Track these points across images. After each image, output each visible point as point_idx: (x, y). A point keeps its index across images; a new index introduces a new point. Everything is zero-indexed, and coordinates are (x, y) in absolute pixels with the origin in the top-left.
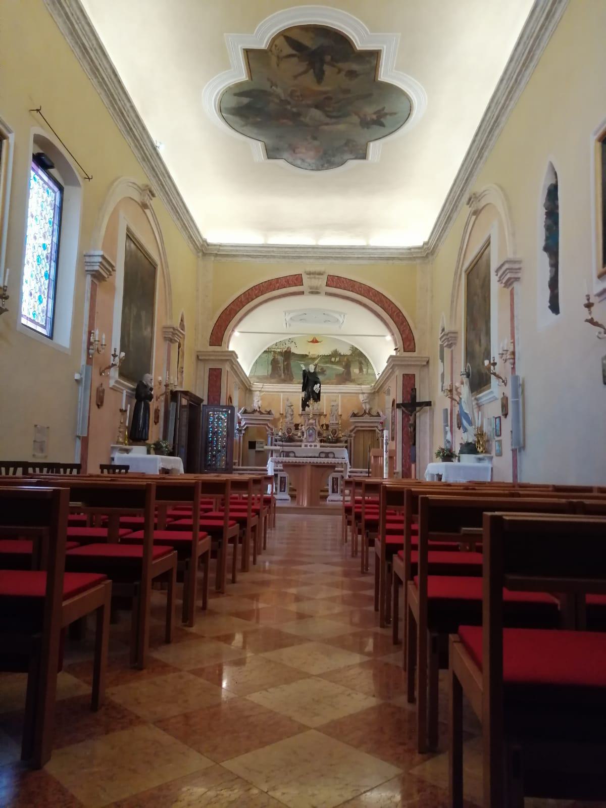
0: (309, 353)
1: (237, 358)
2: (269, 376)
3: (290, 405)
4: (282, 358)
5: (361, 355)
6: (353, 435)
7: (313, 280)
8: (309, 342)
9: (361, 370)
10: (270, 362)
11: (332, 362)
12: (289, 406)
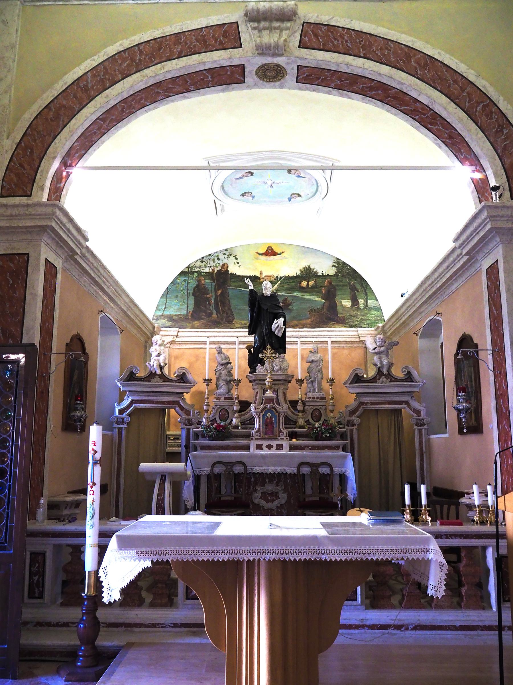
0: (261, 273)
1: (87, 240)
2: (190, 317)
3: (224, 362)
4: (214, 284)
5: (354, 274)
6: (357, 421)
7: (265, 33)
8: (260, 254)
9: (355, 302)
10: (191, 292)
11: (303, 288)
12: (222, 365)
